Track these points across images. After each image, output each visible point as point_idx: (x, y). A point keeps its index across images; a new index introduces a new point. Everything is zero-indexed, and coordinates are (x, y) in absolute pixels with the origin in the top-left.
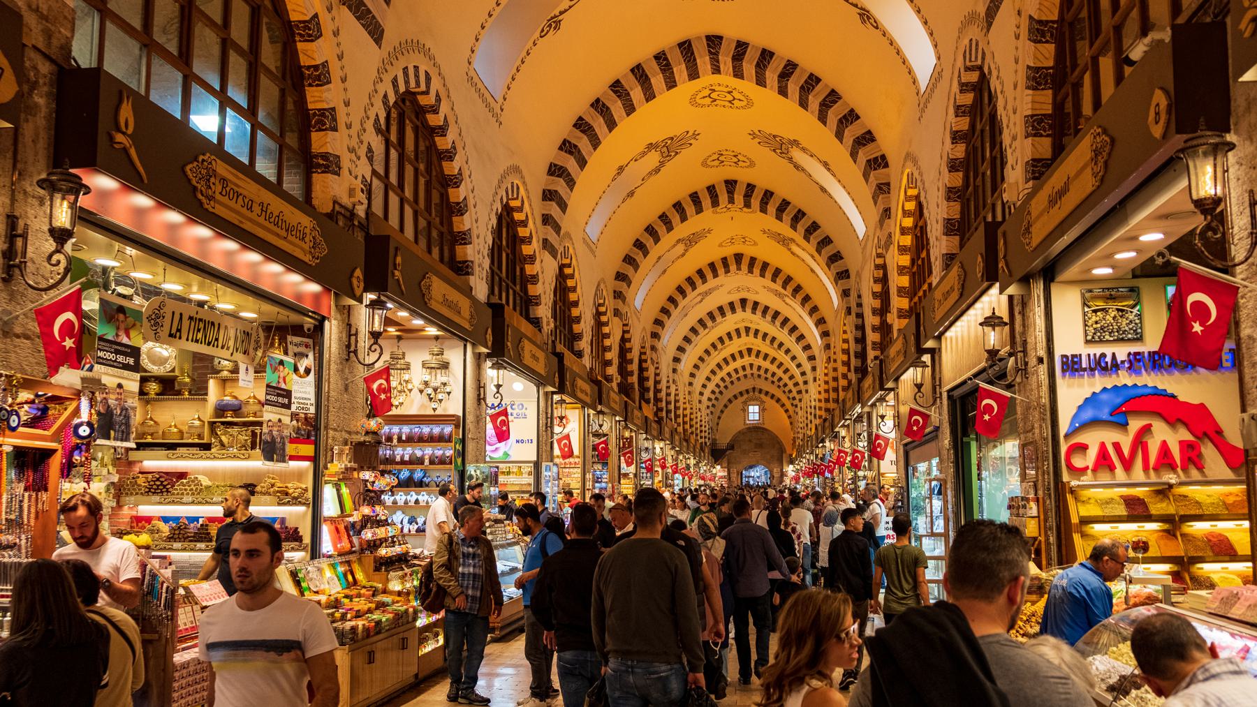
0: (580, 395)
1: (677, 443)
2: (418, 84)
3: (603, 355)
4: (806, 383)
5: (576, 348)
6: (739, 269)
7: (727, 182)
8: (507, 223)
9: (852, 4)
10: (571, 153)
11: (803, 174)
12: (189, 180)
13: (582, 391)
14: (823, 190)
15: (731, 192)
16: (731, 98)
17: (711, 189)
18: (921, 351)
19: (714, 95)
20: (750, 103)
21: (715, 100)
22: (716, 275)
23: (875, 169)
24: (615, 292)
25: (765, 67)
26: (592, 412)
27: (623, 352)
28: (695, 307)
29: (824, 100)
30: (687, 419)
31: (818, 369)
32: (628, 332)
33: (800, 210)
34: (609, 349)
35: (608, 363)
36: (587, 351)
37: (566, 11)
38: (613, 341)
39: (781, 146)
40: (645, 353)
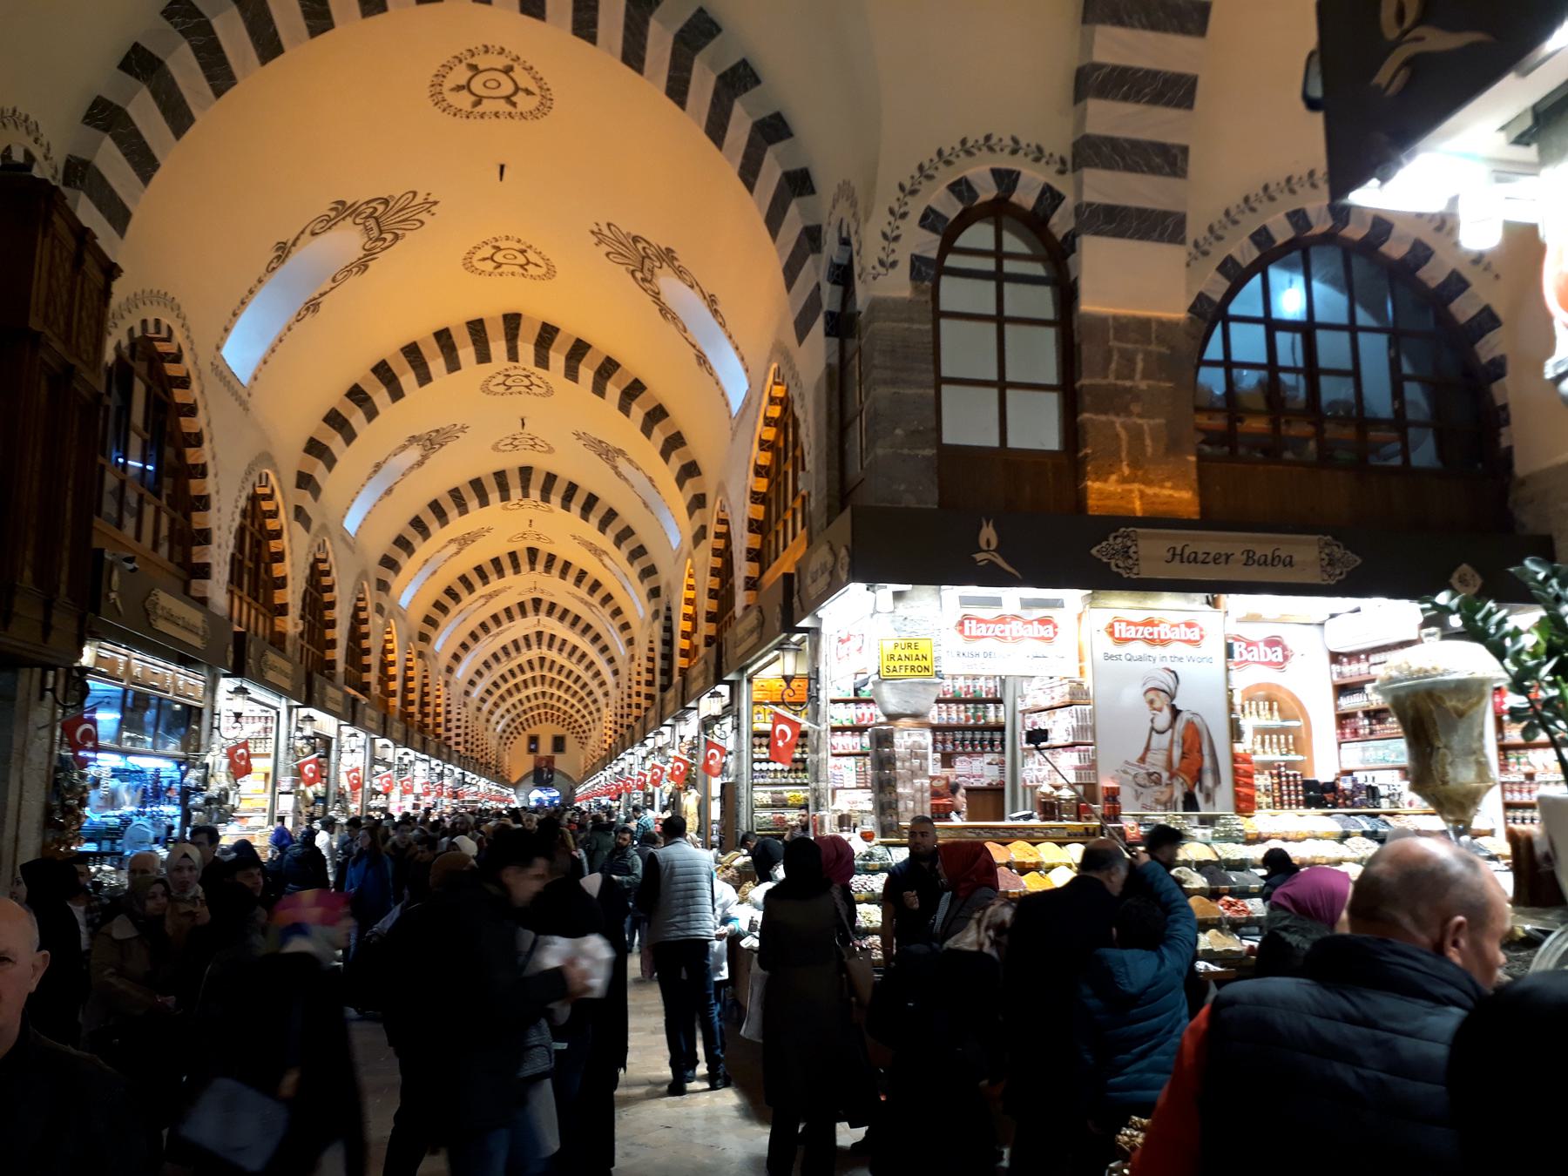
4: (598, 710)
6: (526, 495)
9: (297, 238)
11: (624, 483)
14: (702, 359)
18: (719, 680)
19: (499, 257)
20: (550, 392)
21: (499, 265)
22: (484, 502)
28: (473, 609)
30: (441, 719)
37: (326, 293)
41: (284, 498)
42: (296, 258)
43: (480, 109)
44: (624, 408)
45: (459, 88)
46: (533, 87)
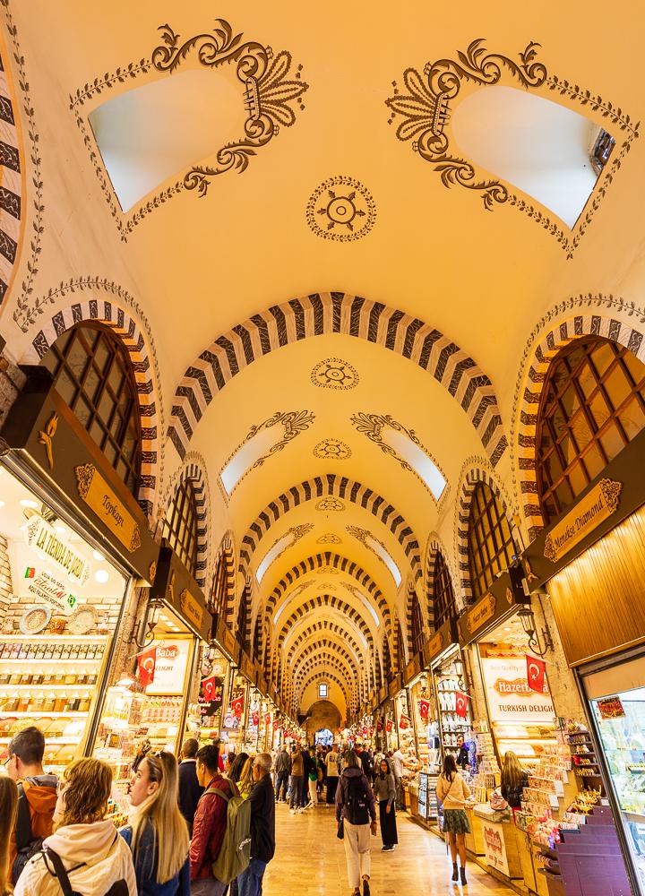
0: (186, 610)
1: (278, 704)
2: (196, 476)
3: (226, 603)
5: (198, 577)
6: (326, 604)
7: (328, 476)
8: (223, 562)
10: (209, 361)
12: (77, 476)
13: (192, 610)
14: (380, 559)
15: (326, 601)
16: (341, 376)
17: (319, 599)
23: (480, 386)
24: (241, 551)
25: (379, 313)
26: (204, 644)
27: (244, 611)
29: (429, 336)
31: (422, 559)
32: (249, 588)
33: (379, 497)
34: (231, 598)
35: (229, 611)
36: (209, 583)
38: (237, 592)
39: (361, 535)
40: (261, 621)
41: (236, 558)
42: (260, 434)
43: (332, 231)
44: (357, 578)
45: (322, 374)
46: (351, 376)
